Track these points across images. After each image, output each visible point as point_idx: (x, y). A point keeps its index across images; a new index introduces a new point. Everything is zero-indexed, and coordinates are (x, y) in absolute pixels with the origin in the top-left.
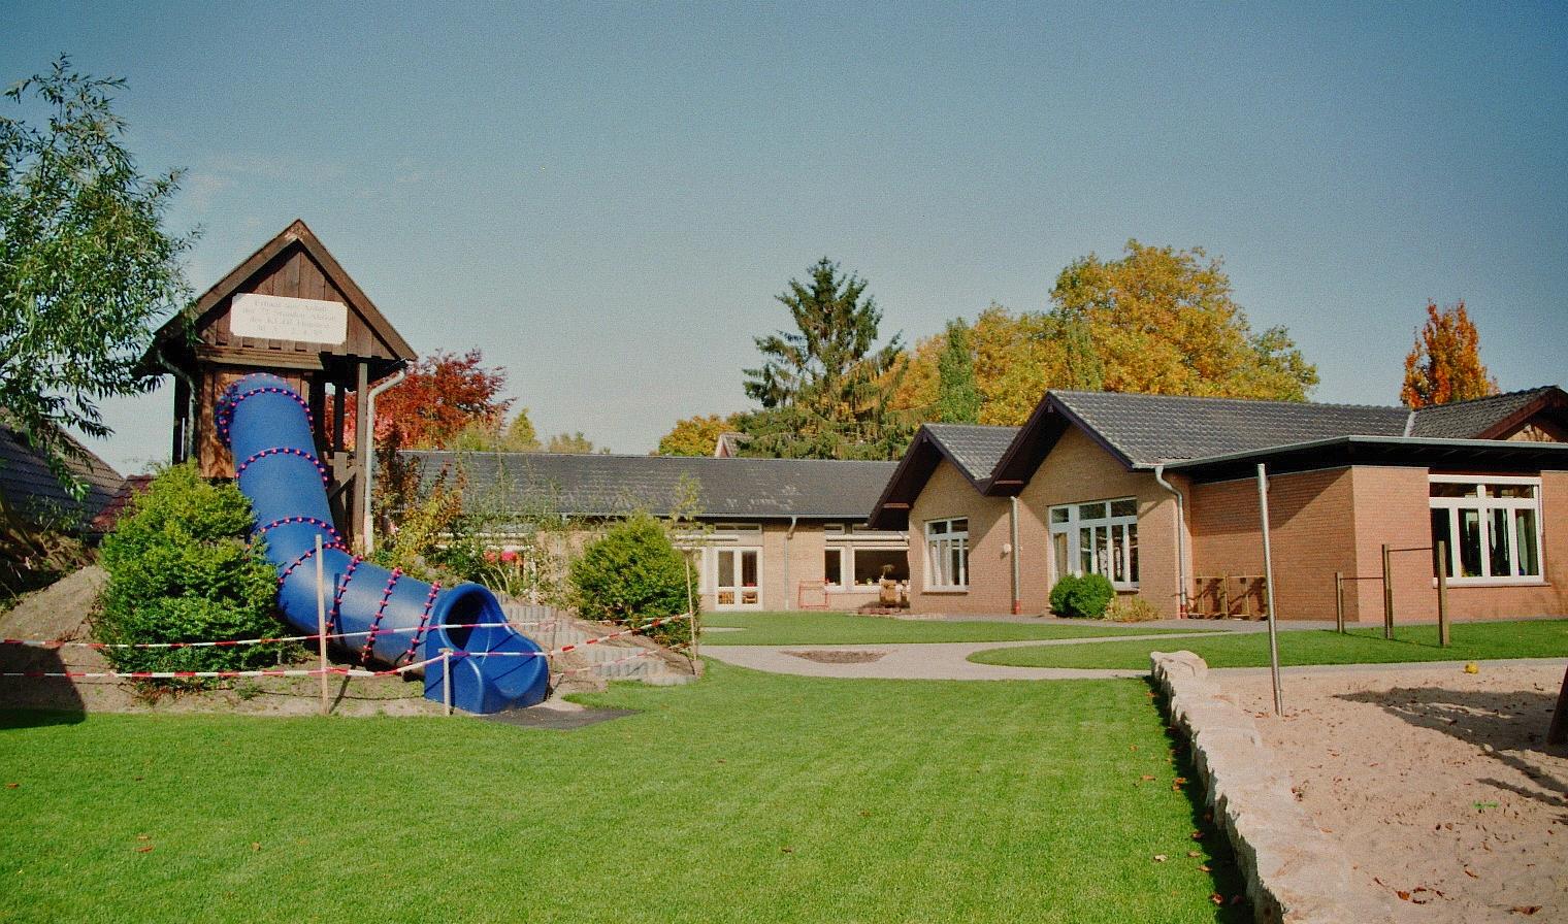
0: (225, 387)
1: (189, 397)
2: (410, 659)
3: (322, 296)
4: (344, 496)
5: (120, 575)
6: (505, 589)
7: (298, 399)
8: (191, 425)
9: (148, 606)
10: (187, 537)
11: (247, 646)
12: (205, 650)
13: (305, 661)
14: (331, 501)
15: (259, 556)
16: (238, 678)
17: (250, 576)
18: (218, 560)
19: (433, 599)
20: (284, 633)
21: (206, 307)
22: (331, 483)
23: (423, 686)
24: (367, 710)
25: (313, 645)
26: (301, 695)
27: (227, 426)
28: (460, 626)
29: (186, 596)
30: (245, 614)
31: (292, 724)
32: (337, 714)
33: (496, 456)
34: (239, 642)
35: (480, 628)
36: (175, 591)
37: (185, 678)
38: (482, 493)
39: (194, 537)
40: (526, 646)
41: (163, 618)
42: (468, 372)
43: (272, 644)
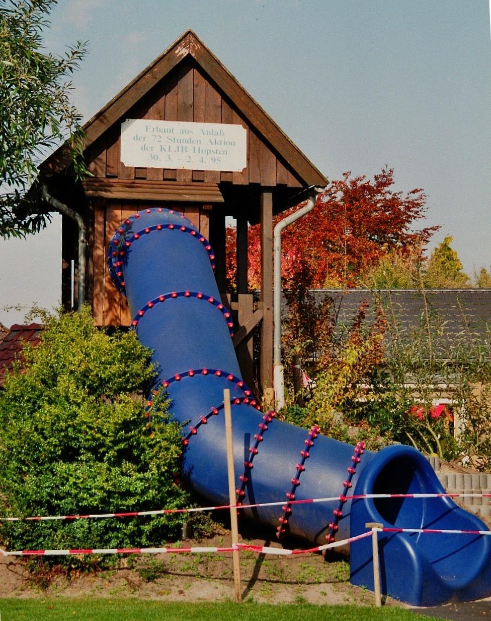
0: (117, 225)
1: (78, 238)
2: (333, 536)
3: (220, 120)
4: (250, 343)
5: (10, 438)
6: (436, 451)
7: (198, 236)
8: (82, 268)
9: (41, 472)
10: (82, 393)
11: (149, 518)
12: (103, 523)
13: (213, 535)
14: (237, 349)
15: (161, 414)
16: (139, 555)
17: (152, 436)
18: (116, 420)
19: (356, 463)
20: (190, 502)
21: (94, 135)
22: (236, 329)
23: (348, 568)
24: (284, 596)
25: (223, 517)
26: (209, 577)
27: (121, 268)
28: (389, 496)
29: (82, 461)
30: (147, 480)
31: (203, 610)
32: (251, 601)
33: (420, 295)
34: (140, 514)
35: (412, 497)
36: (70, 454)
37: (80, 556)
38: (405, 339)
39: (89, 394)
40: (470, 522)
41: (57, 487)
42: (379, 197)
43: (177, 515)
